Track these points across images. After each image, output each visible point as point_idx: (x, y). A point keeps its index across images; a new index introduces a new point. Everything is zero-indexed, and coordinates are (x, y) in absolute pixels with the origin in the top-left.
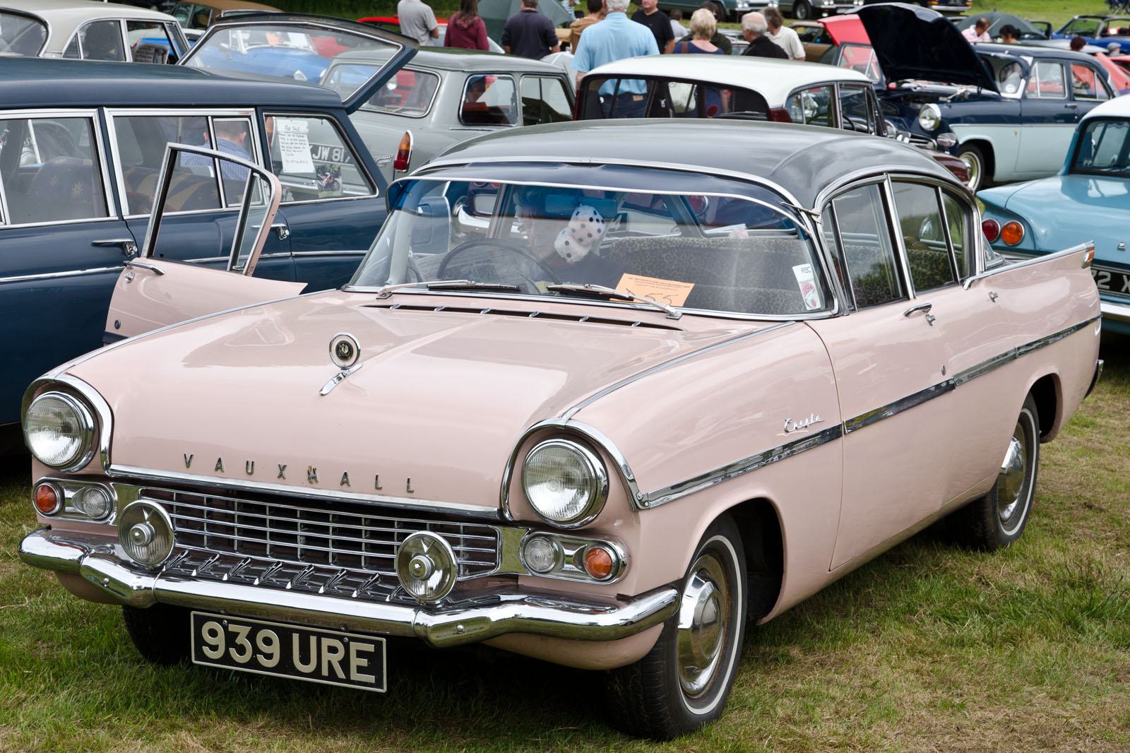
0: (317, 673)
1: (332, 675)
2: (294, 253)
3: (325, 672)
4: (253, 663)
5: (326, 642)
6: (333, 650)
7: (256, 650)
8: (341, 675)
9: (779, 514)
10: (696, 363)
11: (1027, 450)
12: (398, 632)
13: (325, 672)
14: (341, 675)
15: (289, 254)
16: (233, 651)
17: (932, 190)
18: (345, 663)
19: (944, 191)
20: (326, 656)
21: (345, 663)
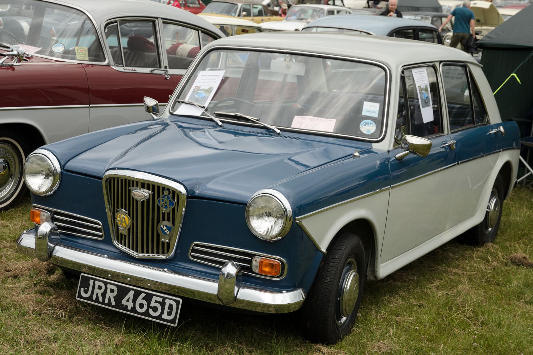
0: (90, 298)
1: (97, 300)
2: (91, 105)
3: (94, 298)
4: (147, 313)
5: (97, 283)
6: (100, 288)
7: (149, 307)
8: (101, 300)
9: (377, 240)
10: (371, 171)
11: (499, 204)
12: (70, 266)
13: (94, 298)
14: (101, 300)
15: (88, 106)
16: (150, 311)
17: (197, 32)
18: (104, 295)
19: (202, 32)
20: (96, 290)
21: (104, 295)
